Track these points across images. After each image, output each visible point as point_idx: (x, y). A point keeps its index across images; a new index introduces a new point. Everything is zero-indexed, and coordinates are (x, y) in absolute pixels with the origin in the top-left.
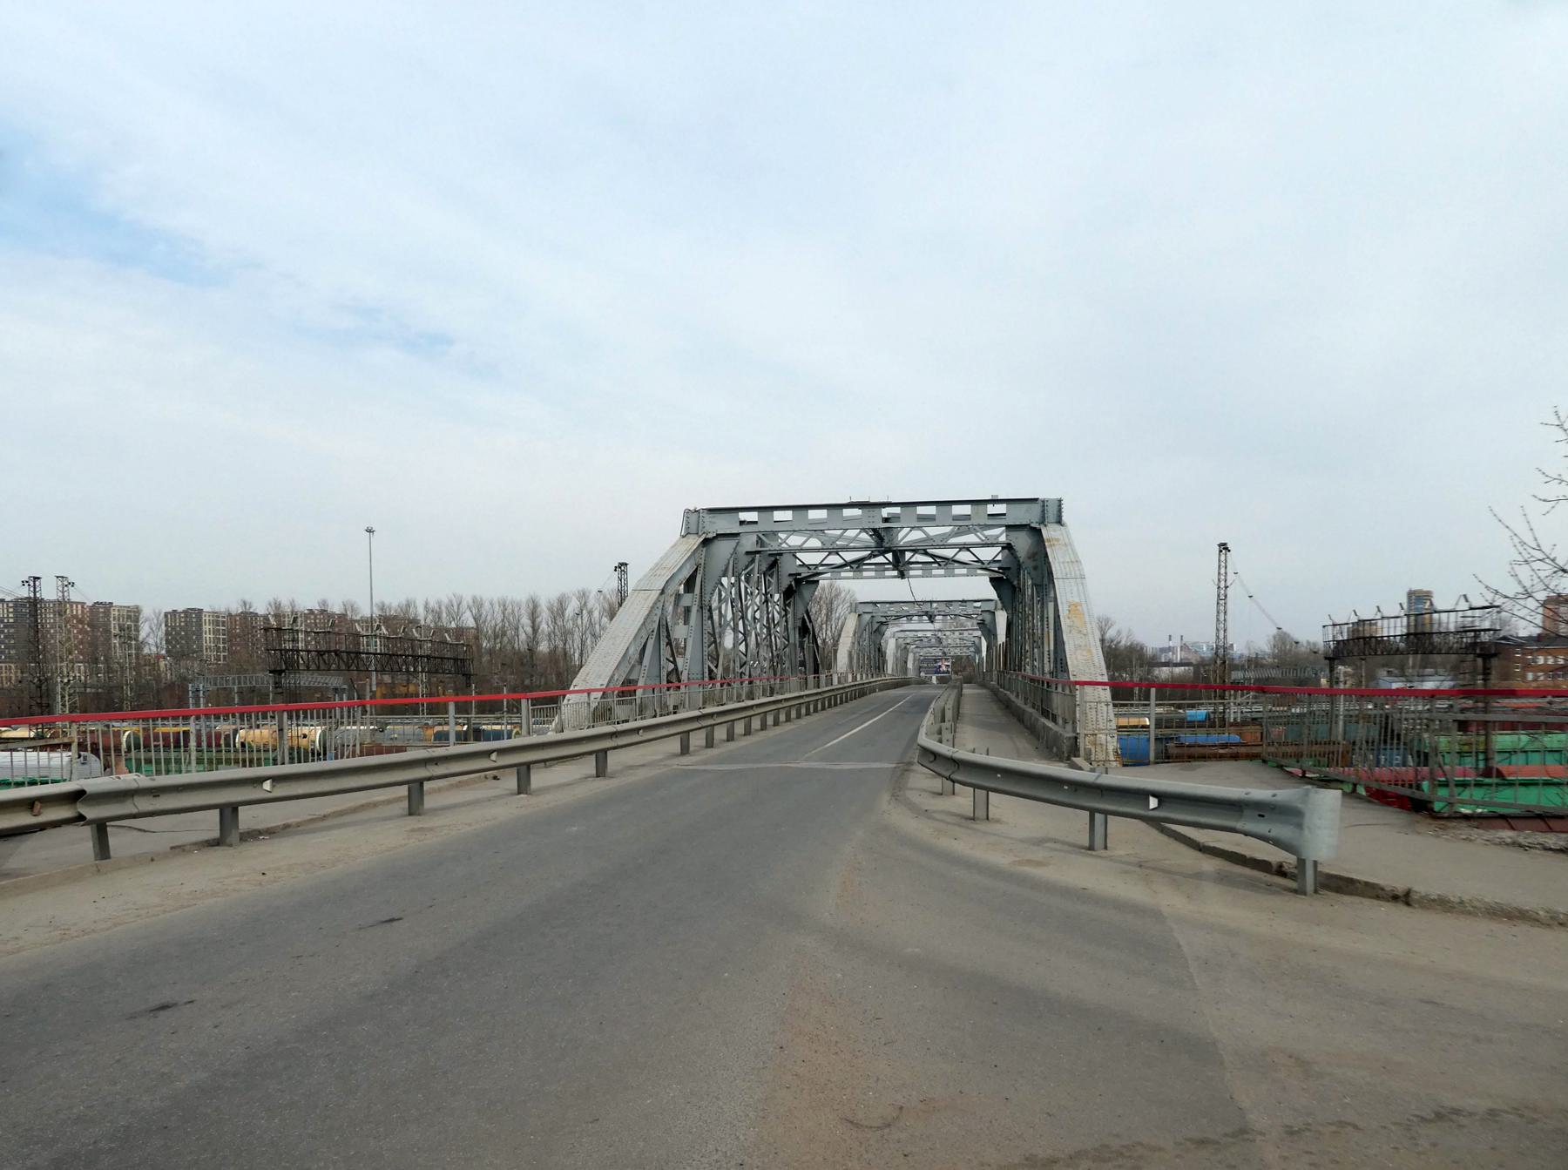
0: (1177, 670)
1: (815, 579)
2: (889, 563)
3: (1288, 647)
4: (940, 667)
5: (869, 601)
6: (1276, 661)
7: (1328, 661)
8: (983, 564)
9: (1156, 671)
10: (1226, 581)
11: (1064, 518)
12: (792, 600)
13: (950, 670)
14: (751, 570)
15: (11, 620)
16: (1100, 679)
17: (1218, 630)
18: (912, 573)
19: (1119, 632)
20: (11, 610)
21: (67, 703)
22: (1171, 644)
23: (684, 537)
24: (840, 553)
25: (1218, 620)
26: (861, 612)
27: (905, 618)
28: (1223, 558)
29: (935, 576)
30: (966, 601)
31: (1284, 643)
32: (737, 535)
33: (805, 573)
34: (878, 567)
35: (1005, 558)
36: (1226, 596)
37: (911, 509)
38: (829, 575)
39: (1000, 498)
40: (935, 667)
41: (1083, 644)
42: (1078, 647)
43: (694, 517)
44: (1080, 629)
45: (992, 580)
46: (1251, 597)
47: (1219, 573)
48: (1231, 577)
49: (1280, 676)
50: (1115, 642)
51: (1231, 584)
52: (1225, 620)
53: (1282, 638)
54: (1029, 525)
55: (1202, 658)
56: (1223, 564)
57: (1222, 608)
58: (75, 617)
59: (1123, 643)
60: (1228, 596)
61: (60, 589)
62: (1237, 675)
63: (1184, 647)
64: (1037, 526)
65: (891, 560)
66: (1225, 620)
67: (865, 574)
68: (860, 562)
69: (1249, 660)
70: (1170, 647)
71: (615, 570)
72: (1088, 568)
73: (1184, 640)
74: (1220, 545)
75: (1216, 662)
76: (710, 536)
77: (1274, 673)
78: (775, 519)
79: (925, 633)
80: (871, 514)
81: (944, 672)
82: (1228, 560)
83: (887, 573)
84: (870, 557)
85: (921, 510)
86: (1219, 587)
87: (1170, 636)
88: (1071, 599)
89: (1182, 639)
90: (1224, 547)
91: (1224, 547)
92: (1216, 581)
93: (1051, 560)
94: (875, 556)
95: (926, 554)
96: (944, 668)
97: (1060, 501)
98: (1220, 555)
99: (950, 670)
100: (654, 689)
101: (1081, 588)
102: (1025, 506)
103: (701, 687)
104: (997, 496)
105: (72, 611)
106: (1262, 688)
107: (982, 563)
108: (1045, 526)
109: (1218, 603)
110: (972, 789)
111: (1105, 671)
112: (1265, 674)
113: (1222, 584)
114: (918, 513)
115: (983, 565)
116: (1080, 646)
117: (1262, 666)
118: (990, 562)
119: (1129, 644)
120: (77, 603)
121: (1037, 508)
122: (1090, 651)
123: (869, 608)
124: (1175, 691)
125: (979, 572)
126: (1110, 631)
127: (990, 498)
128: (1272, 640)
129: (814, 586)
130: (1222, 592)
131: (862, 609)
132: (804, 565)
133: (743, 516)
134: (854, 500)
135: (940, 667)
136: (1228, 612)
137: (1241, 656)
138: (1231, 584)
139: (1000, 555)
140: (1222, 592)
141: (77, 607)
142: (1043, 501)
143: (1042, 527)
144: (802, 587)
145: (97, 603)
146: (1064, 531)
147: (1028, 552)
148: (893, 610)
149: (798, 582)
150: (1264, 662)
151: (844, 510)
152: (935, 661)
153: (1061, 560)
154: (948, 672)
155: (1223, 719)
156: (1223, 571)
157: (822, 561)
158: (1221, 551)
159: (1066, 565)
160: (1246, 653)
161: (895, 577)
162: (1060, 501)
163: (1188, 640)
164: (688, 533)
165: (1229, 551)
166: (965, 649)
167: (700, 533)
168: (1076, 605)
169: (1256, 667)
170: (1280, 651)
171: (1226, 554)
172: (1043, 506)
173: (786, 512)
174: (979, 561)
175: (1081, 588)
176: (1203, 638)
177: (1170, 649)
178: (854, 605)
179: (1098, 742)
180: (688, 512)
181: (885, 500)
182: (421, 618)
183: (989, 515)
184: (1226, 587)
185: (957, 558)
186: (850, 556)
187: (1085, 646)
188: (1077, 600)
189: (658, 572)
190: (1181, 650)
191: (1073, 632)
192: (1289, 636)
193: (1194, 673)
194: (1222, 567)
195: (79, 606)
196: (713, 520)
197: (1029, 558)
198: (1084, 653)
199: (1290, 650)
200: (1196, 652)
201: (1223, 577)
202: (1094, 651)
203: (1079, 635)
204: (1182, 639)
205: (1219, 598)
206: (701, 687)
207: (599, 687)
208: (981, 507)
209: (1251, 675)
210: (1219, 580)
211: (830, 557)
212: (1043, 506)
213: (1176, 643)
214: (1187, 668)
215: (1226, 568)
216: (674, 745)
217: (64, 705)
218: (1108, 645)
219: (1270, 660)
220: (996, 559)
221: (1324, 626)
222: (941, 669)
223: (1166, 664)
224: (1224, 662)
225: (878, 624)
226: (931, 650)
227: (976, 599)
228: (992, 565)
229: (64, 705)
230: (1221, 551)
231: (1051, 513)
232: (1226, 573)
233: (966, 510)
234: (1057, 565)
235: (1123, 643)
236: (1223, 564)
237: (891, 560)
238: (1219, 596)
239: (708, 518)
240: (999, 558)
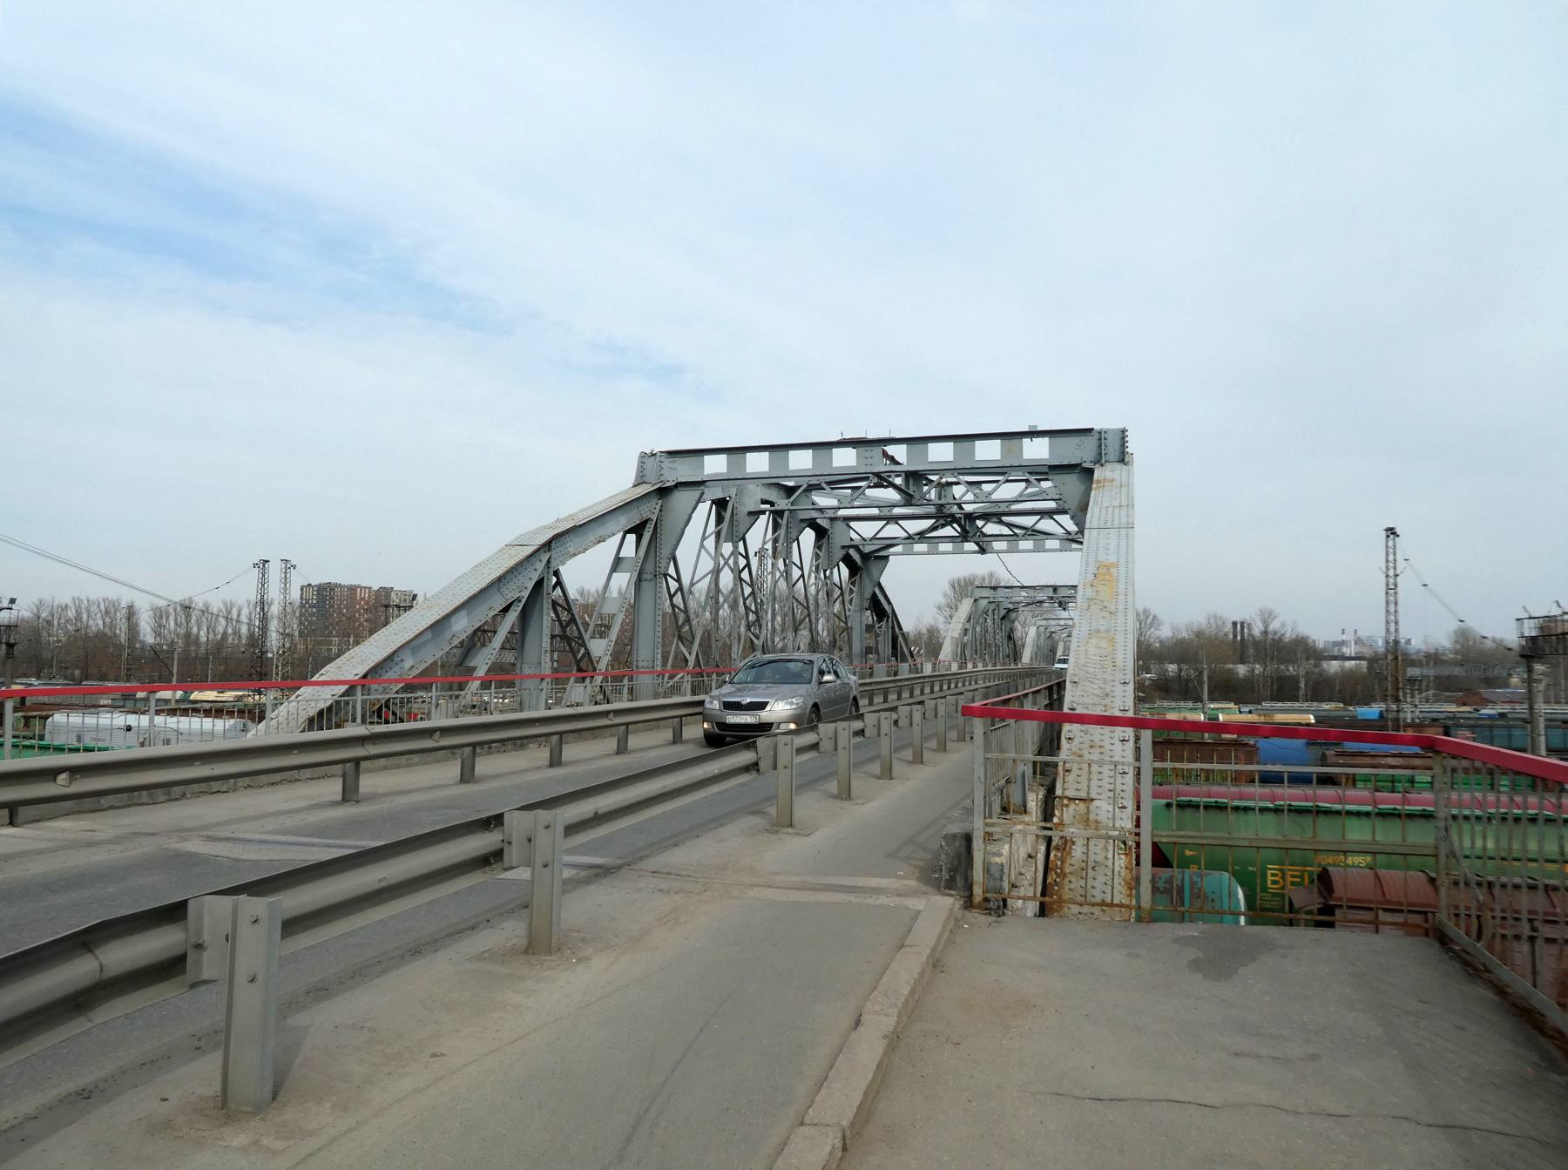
0: (1349, 664)
6: (1459, 657)
7: (1523, 660)
9: (1325, 665)
10: (1395, 568)
12: (858, 577)
14: (779, 535)
15: (314, 602)
17: (1387, 622)
19: (1283, 625)
20: (315, 593)
21: (280, 673)
22: (1344, 637)
25: (1387, 611)
26: (977, 598)
28: (1391, 543)
36: (1396, 585)
39: (1039, 429)
41: (1103, 628)
46: (1425, 585)
47: (1387, 561)
48: (1401, 565)
49: (1464, 674)
50: (1279, 635)
52: (1396, 612)
53: (1463, 635)
55: (1376, 653)
56: (1391, 551)
57: (1392, 598)
58: (362, 599)
59: (1288, 635)
60: (1399, 586)
61: (284, 570)
62: (1413, 672)
63: (1358, 641)
66: (1396, 612)
68: (921, 536)
69: (1428, 656)
70: (1343, 641)
71: (756, 556)
72: (1140, 516)
73: (1359, 634)
75: (1387, 658)
77: (1457, 671)
80: (869, 454)
82: (1397, 546)
84: (933, 528)
86: (1387, 576)
87: (1343, 630)
88: (1102, 557)
89: (1356, 633)
90: (1391, 532)
91: (1391, 532)
92: (1384, 569)
97: (1124, 431)
98: (1387, 541)
101: (1123, 543)
102: (1075, 440)
104: (1036, 426)
105: (361, 594)
106: (1446, 686)
109: (1387, 593)
112: (1446, 672)
113: (1391, 573)
116: (1098, 631)
117: (1443, 662)
119: (1294, 636)
120: (365, 588)
121: (1090, 443)
122: (1112, 641)
123: (986, 593)
124: (1352, 689)
126: (1274, 622)
129: (883, 562)
130: (1392, 581)
131: (979, 593)
134: (847, 436)
137: (1419, 651)
140: (1392, 581)
141: (361, 590)
144: (869, 563)
145: (381, 588)
146: (1124, 473)
149: (1009, 611)
150: (1445, 658)
155: (1397, 720)
156: (1391, 558)
157: (876, 534)
158: (1388, 536)
160: (1423, 647)
161: (975, 552)
162: (1124, 431)
163: (1362, 634)
165: (1398, 536)
169: (1435, 663)
170: (1463, 646)
171: (1394, 540)
173: (762, 453)
175: (1123, 543)
176: (1374, 632)
177: (1343, 643)
179: (1092, 817)
180: (643, 456)
181: (887, 436)
182: (1186, 637)
184: (1396, 576)
187: (1108, 631)
188: (1112, 559)
190: (1355, 644)
193: (1368, 668)
194: (1390, 557)
195: (367, 590)
198: (1103, 644)
200: (1371, 646)
201: (1391, 565)
202: (1120, 639)
204: (1356, 633)
205: (1388, 588)
209: (1431, 672)
210: (1387, 568)
211: (888, 526)
213: (1349, 637)
214: (1358, 662)
215: (1395, 555)
216: (334, 788)
217: (277, 674)
218: (1270, 637)
219: (1452, 656)
221: (1518, 620)
223: (1335, 658)
224: (1396, 658)
225: (1006, 611)
229: (277, 674)
230: (1388, 536)
232: (1395, 560)
235: (1288, 635)
236: (1391, 551)
238: (1387, 585)
239: (667, 462)
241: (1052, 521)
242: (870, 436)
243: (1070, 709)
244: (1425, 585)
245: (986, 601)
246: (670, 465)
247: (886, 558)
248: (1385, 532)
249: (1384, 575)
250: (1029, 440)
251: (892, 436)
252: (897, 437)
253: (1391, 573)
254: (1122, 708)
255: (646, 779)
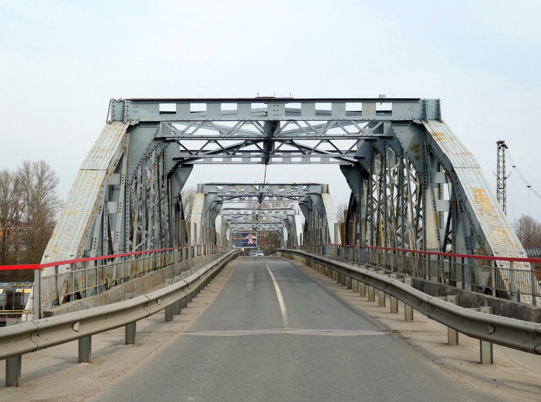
1: (190, 163)
2: (261, 151)
3: (532, 230)
4: (248, 240)
5: (210, 183)
8: (342, 153)
10: (504, 173)
11: (443, 117)
13: (256, 243)
16: (520, 256)
18: (274, 159)
23: (110, 123)
24: (218, 141)
26: (207, 193)
27: (237, 199)
28: (501, 153)
29: (294, 163)
30: (296, 185)
31: (529, 227)
32: (158, 123)
33: (186, 156)
34: (286, 155)
35: (360, 149)
37: (309, 105)
38: (202, 160)
39: (387, 97)
40: (244, 240)
42: (493, 228)
43: (119, 106)
44: (490, 212)
45: (342, 167)
46: (529, 187)
48: (509, 169)
51: (509, 176)
54: (412, 121)
56: (501, 159)
64: (419, 122)
65: (262, 148)
67: (293, 159)
74: (500, 143)
76: (133, 123)
78: (191, 111)
79: (238, 211)
80: (276, 108)
81: (251, 245)
83: (253, 160)
85: (319, 106)
86: (498, 178)
90: (502, 145)
91: (502, 145)
92: (496, 173)
93: (444, 151)
94: (247, 145)
95: (293, 144)
96: (251, 241)
98: (498, 150)
99: (256, 243)
100: (96, 262)
101: (479, 177)
102: (408, 105)
103: (123, 258)
107: (341, 152)
108: (427, 122)
110: (478, 341)
111: (523, 250)
113: (501, 176)
114: (286, 107)
115: (338, 154)
116: (494, 227)
118: (347, 152)
121: (418, 107)
122: (504, 231)
125: (331, 160)
127: (378, 97)
128: (519, 223)
129: (189, 169)
130: (501, 182)
131: (207, 189)
132: (186, 150)
133: (164, 107)
134: (262, 95)
135: (248, 240)
136: (507, 199)
138: (509, 176)
139: (356, 146)
140: (501, 182)
142: (424, 101)
143: (424, 123)
147: (411, 144)
148: (228, 192)
151: (252, 104)
152: (245, 235)
153: (454, 152)
154: (254, 245)
156: (501, 164)
158: (500, 148)
159: (459, 155)
161: (259, 163)
162: (438, 101)
164: (114, 120)
165: (507, 148)
166: (273, 226)
167: (125, 121)
168: (480, 191)
171: (503, 151)
172: (424, 105)
174: (338, 151)
175: (479, 177)
178: (201, 186)
183: (377, 112)
184: (505, 178)
185: (318, 148)
186: (226, 144)
188: (479, 187)
189: (99, 154)
191: (484, 214)
192: (532, 220)
194: (501, 162)
196: (137, 109)
197: (412, 149)
198: (500, 233)
199: (534, 232)
201: (501, 170)
203: (491, 218)
206: (123, 258)
207: (69, 258)
208: (370, 105)
210: (498, 172)
212: (424, 105)
215: (504, 162)
220: (352, 149)
222: (249, 242)
226: (245, 225)
227: (301, 183)
228: (349, 154)
231: (431, 112)
232: (504, 166)
233: (358, 107)
234: (452, 156)
237: (262, 148)
238: (498, 185)
239: (131, 107)
240: (355, 148)
241: (329, 143)
242: (277, 96)
243: (501, 266)
244: (529, 187)
245: (213, 196)
246: (133, 109)
247: (192, 166)
248: (497, 144)
249: (497, 177)
250: (380, 103)
251: (292, 97)
252: (295, 98)
253: (501, 176)
254: (525, 265)
255: (62, 341)
